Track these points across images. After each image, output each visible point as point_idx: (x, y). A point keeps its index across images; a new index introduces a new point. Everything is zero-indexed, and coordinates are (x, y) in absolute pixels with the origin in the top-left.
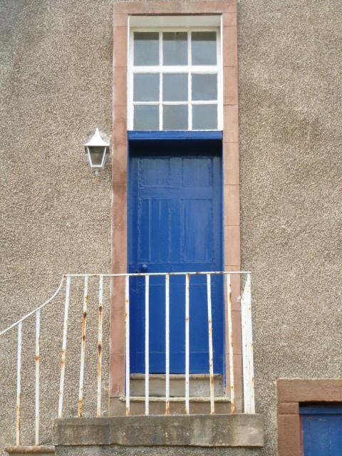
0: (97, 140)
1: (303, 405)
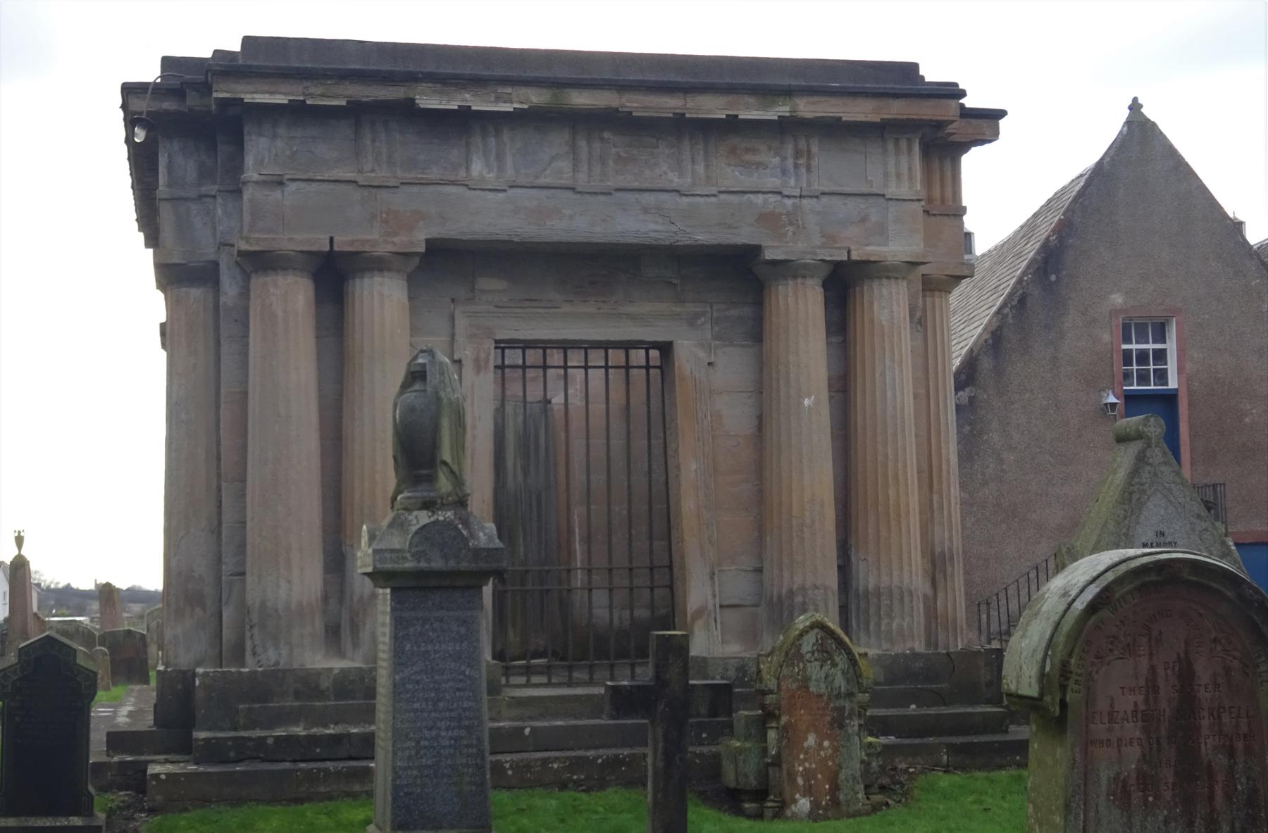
0: (1112, 399)
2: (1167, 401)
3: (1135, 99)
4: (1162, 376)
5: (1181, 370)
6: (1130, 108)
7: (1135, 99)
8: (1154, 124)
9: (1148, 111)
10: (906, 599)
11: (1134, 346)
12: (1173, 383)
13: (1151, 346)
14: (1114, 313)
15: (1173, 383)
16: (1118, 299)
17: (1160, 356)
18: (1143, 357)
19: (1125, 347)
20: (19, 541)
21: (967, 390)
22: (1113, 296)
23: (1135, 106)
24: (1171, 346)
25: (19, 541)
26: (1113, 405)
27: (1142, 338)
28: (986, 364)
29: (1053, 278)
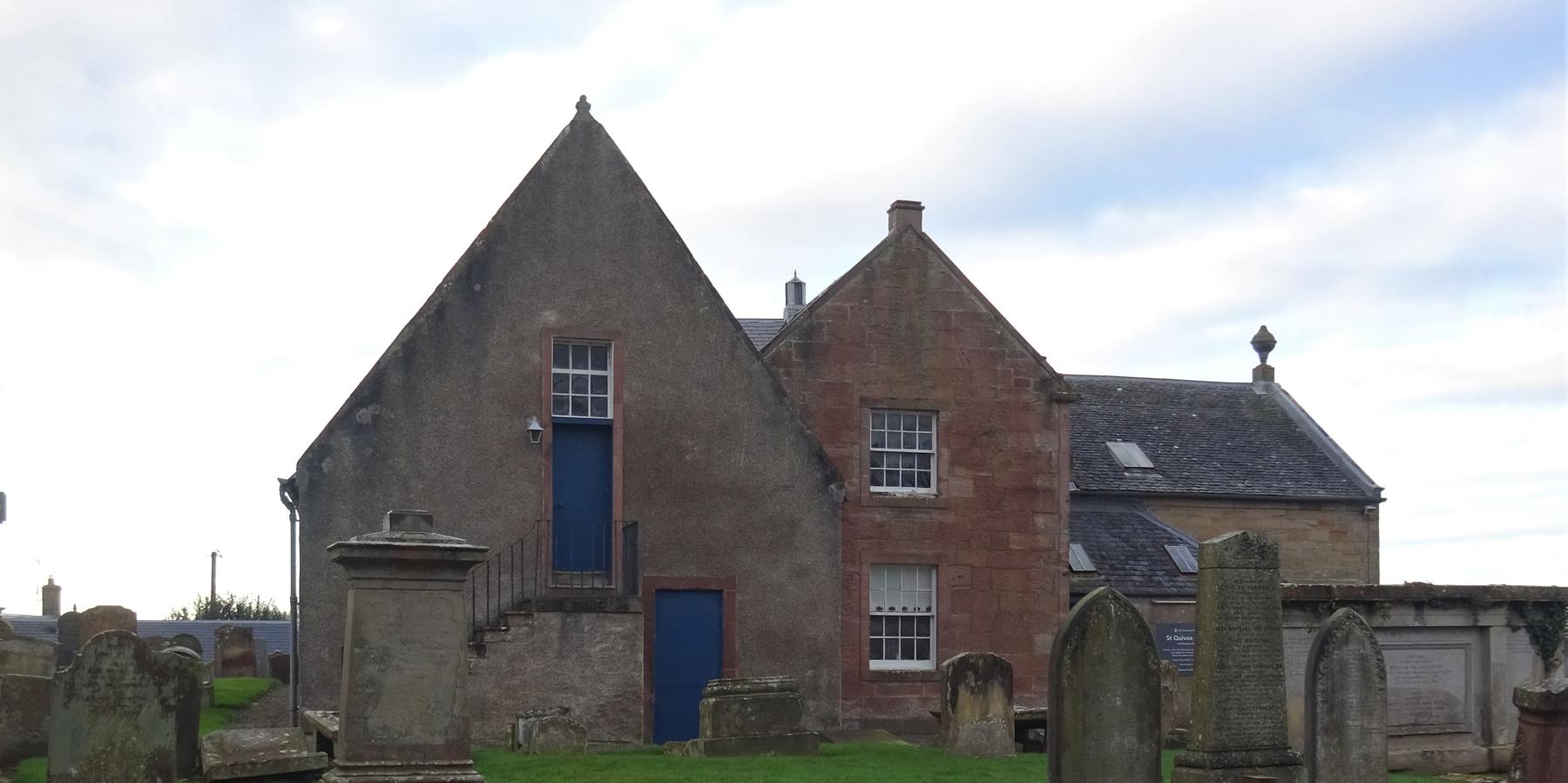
0: (535, 426)
1: (658, 591)
2: (606, 429)
3: (583, 98)
4: (601, 405)
5: (617, 399)
6: (578, 106)
7: (583, 98)
8: (600, 126)
9: (596, 113)
10: (517, 564)
11: (571, 371)
12: (610, 416)
13: (590, 372)
14: (547, 331)
15: (610, 416)
16: (550, 317)
17: (600, 383)
18: (580, 381)
19: (555, 370)
20: (1264, 343)
21: (371, 408)
22: (546, 313)
23: (583, 105)
24: (610, 373)
25: (1264, 343)
26: (535, 433)
27: (580, 362)
28: (395, 378)
29: (477, 287)
